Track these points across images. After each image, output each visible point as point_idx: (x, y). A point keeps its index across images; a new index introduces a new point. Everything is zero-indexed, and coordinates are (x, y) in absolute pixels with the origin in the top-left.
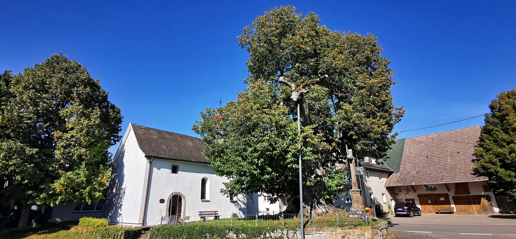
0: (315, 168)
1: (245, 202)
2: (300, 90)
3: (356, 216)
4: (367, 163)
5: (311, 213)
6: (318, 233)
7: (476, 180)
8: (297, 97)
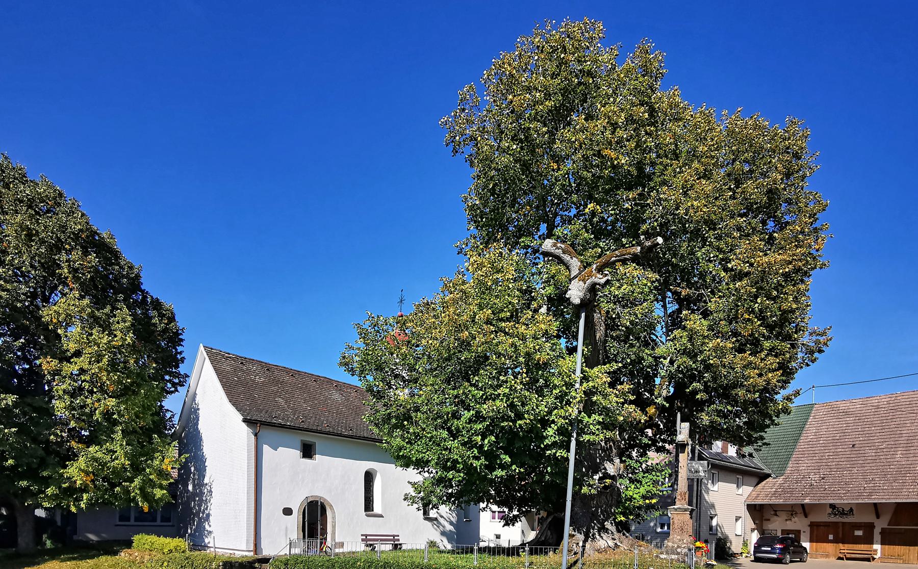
2: (590, 276)
3: (673, 557)
4: (718, 454)
5: (584, 546)
8: (581, 294)
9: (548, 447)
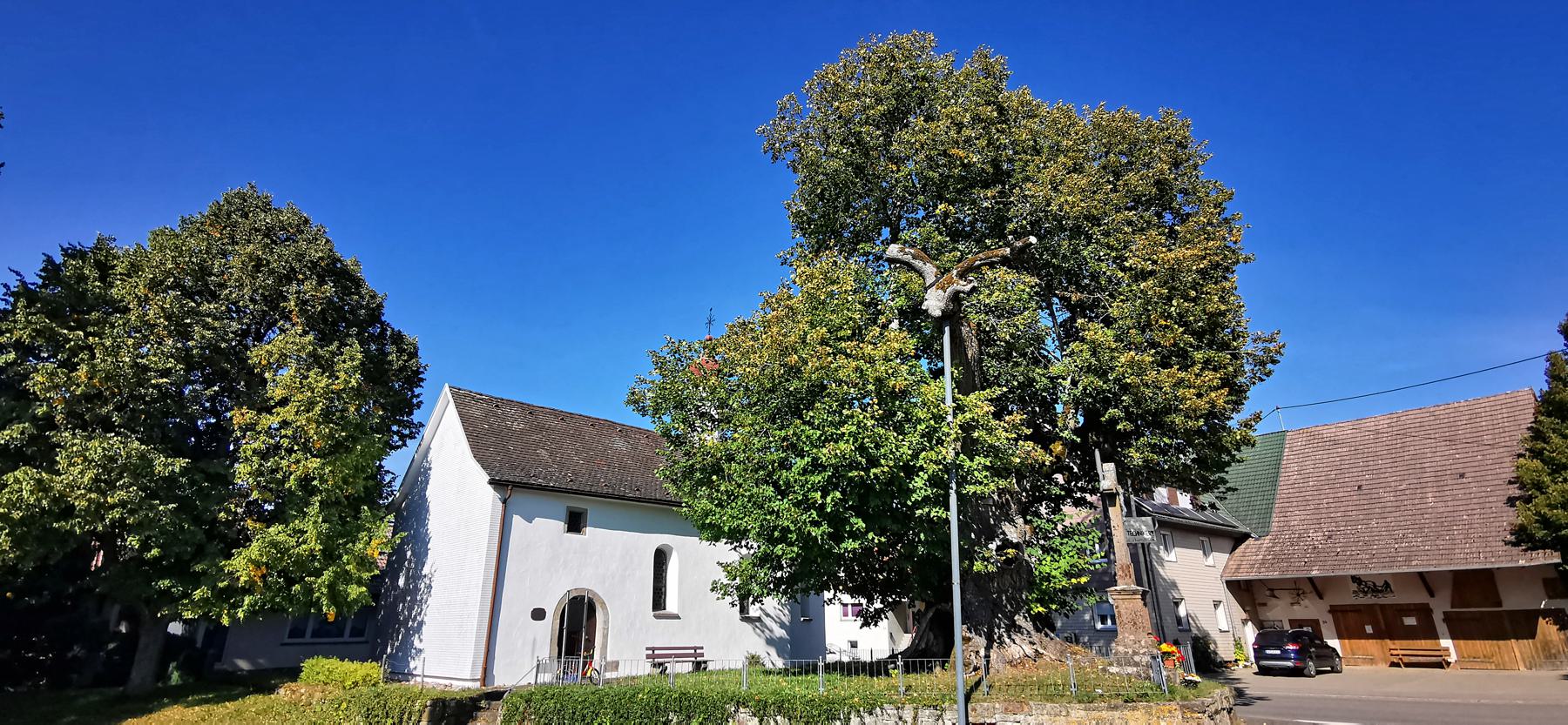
0: (998, 520)
1: (786, 620)
2: (951, 282)
3: (1130, 670)
4: (1164, 506)
5: (987, 656)
6: (1012, 718)
7: (1522, 563)
8: (942, 305)
9: (917, 505)
